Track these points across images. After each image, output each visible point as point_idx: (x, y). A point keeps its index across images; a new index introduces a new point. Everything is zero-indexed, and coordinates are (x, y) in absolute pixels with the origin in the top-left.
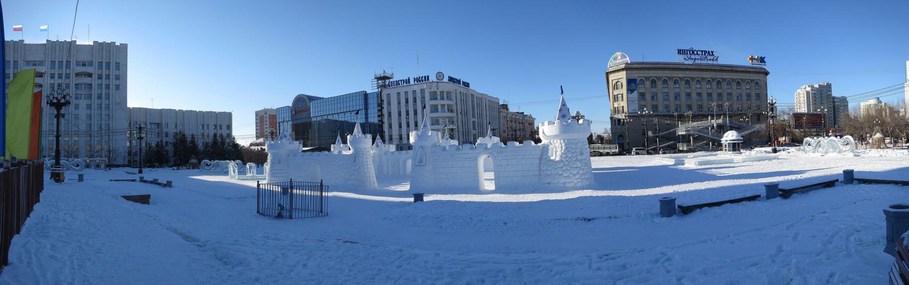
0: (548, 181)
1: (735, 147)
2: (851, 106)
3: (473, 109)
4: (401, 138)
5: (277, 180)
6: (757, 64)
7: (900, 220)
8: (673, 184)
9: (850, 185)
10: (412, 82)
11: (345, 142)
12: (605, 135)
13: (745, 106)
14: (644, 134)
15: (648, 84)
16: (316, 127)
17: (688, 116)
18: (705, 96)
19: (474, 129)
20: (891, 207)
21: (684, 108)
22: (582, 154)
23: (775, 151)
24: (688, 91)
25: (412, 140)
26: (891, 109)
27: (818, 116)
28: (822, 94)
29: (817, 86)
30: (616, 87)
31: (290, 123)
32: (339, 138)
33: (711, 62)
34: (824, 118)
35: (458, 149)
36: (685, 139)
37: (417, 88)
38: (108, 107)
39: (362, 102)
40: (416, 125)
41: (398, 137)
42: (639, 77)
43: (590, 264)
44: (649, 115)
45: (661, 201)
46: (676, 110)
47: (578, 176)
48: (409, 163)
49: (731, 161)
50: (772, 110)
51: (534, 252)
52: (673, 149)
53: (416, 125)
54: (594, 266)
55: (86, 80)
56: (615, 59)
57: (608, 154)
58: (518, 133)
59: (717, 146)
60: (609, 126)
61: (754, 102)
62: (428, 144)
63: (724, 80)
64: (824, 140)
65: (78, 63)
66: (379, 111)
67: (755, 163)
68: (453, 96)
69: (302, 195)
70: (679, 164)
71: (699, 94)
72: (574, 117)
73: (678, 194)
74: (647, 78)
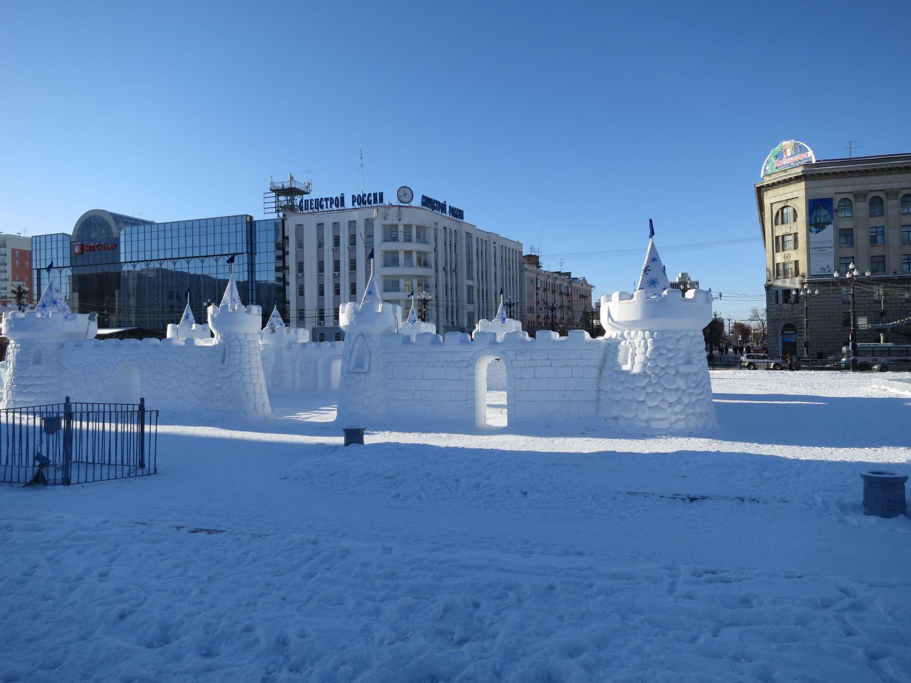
0: (616, 413)
3: (470, 262)
4: (321, 317)
5: (31, 401)
10: (348, 203)
11: (201, 319)
12: (754, 325)
14: (846, 323)
15: (861, 208)
16: (132, 284)
19: (470, 301)
22: (689, 362)
25: (344, 320)
30: (780, 218)
31: (69, 272)
32: (188, 310)
35: (435, 342)
37: (359, 216)
39: (242, 237)
40: (353, 291)
41: (315, 313)
43: (673, 584)
44: (861, 281)
47: (678, 408)
48: (337, 367)
51: (580, 554)
53: (353, 291)
56: (778, 156)
58: (558, 315)
60: (762, 305)
62: (375, 329)
66: (278, 258)
68: (430, 234)
69: (94, 432)
72: (674, 286)
74: (859, 196)
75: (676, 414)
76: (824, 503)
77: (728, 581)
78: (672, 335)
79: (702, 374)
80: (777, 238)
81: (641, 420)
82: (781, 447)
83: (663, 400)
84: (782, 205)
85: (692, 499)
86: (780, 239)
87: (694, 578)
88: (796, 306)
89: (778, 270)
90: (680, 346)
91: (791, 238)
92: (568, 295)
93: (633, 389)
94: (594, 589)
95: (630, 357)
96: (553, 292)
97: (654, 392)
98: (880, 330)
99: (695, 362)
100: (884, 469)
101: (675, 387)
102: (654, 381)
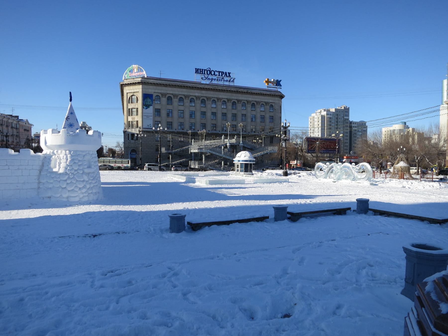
0: (49, 195)
1: (247, 168)
2: (370, 131)
6: (273, 87)
7: (421, 261)
8: (183, 201)
9: (364, 215)
12: (117, 149)
13: (259, 128)
14: (157, 150)
15: (164, 100)
17: (202, 135)
18: (219, 116)
20: (413, 246)
21: (198, 126)
22: (89, 167)
23: (286, 174)
24: (204, 110)
26: (421, 135)
27: (332, 142)
28: (338, 119)
29: (333, 110)
30: (130, 100)
33: (227, 83)
34: (341, 142)
36: (197, 157)
42: (156, 93)
43: (93, 282)
44: (163, 132)
45: (171, 217)
46: (191, 128)
47: (84, 190)
49: (242, 182)
50: (285, 133)
51: (35, 275)
52: (184, 166)
54: (97, 284)
56: (131, 71)
57: (119, 168)
58: (10, 139)
59: (229, 166)
60: (121, 140)
61: (268, 124)
63: (239, 101)
64: (337, 166)
67: (266, 185)
70: (190, 182)
71: (214, 114)
73: (188, 211)
74: (164, 95)
75: (83, 193)
76: (154, 230)
77: (120, 275)
78: (81, 153)
79: (96, 173)
80: (129, 109)
81: (63, 198)
82: (133, 206)
83: (76, 187)
84: (132, 94)
85: (95, 236)
86: (131, 110)
87: (103, 277)
88: (136, 141)
89: (129, 124)
90: (85, 159)
91: (135, 110)
92: (17, 128)
93: (59, 182)
94: (49, 295)
95: (58, 164)
96: (7, 126)
97: (71, 182)
98: (170, 153)
99: (93, 167)
100: (178, 213)
101: (82, 180)
102: (71, 177)
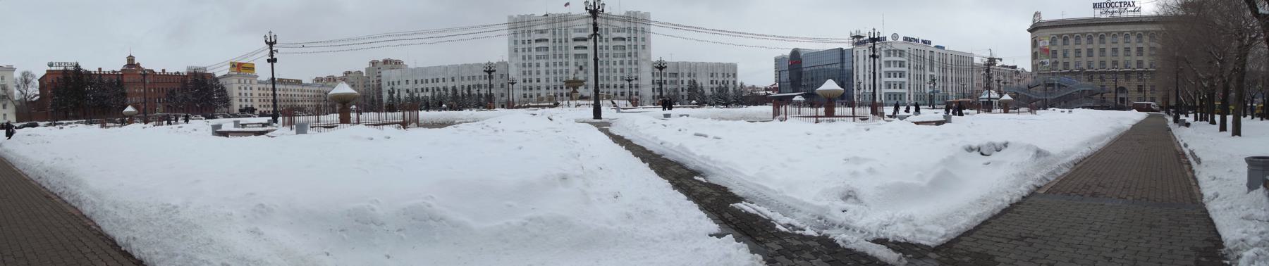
33: (1131, 14)
38: (636, 63)
55: (621, 43)
65: (576, 31)
